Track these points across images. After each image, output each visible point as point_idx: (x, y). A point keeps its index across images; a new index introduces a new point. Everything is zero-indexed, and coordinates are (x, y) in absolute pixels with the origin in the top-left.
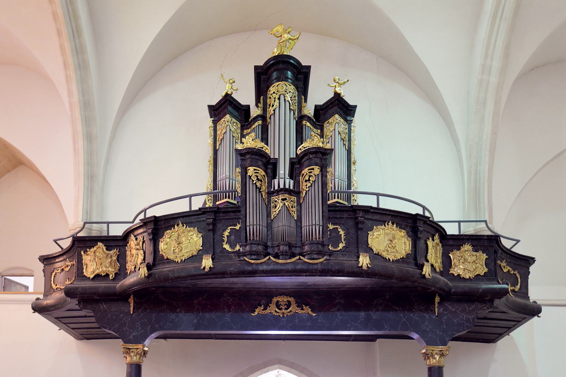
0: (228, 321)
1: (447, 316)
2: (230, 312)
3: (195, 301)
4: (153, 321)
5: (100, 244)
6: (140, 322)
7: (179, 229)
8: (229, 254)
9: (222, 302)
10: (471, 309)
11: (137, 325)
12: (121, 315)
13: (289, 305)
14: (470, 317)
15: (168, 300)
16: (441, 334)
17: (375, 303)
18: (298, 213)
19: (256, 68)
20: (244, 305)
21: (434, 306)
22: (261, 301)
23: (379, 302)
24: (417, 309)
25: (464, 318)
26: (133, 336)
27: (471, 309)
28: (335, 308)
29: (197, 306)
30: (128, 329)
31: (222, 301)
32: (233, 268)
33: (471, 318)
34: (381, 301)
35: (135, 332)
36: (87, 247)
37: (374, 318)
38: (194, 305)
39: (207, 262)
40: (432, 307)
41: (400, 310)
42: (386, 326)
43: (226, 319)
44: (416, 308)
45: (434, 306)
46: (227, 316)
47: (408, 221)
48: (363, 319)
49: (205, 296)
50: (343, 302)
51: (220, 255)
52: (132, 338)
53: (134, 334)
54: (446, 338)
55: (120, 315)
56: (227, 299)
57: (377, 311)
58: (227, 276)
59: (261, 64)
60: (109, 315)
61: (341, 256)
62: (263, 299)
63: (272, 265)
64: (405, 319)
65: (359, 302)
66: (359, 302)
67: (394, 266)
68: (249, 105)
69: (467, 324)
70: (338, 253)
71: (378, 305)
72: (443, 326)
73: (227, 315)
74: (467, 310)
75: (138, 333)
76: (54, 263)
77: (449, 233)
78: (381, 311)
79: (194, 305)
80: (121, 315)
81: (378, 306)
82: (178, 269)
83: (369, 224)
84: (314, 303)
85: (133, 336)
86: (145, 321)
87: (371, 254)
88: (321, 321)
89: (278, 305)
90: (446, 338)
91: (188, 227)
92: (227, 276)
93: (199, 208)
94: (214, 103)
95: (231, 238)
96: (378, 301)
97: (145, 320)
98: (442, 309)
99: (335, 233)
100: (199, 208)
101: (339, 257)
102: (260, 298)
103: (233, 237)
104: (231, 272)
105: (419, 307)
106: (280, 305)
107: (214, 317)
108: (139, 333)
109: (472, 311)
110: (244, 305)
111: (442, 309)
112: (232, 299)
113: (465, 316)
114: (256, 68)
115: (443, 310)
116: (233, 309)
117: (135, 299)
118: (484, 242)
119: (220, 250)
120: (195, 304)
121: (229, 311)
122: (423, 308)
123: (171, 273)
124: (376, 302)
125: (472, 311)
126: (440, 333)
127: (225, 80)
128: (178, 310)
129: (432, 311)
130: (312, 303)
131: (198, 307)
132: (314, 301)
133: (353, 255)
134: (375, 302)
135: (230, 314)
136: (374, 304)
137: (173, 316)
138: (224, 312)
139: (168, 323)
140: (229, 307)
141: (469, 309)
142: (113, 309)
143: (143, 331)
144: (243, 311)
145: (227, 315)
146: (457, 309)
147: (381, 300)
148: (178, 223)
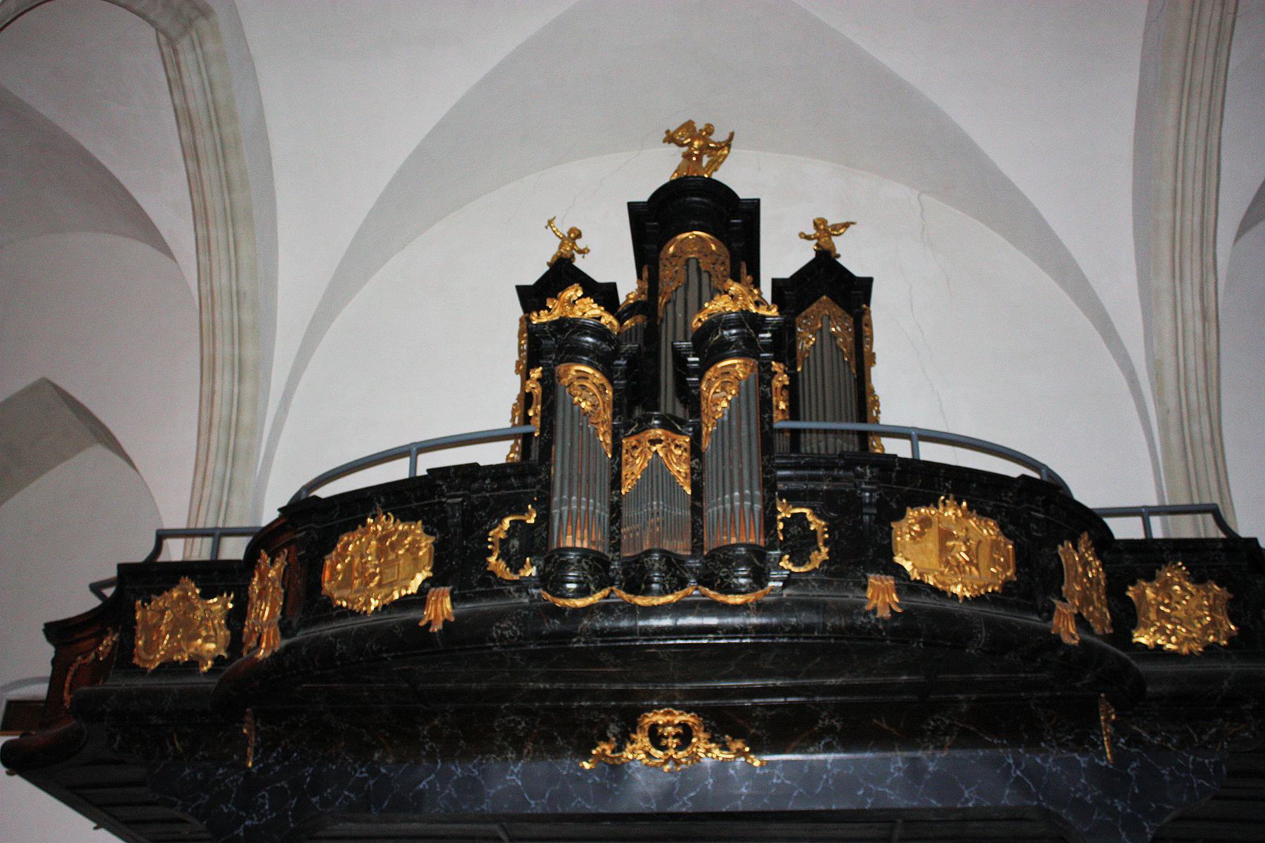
0: (514, 784)
1: (1138, 761)
2: (522, 758)
3: (421, 728)
4: (305, 787)
5: (185, 580)
6: (268, 788)
7: (379, 525)
8: (502, 588)
9: (498, 730)
10: (1205, 738)
11: (260, 797)
12: (221, 771)
13: (685, 736)
14: (1207, 761)
15: (347, 726)
16: (1129, 811)
17: (931, 728)
18: (694, 478)
19: (632, 207)
20: (559, 738)
21: (1099, 733)
22: (607, 727)
23: (943, 723)
24: (1050, 741)
25: (1188, 764)
26: (246, 828)
27: (1205, 738)
28: (817, 744)
29: (428, 742)
30: (234, 809)
31: (498, 726)
32: (509, 622)
33: (1210, 763)
34: (947, 722)
35: (252, 819)
36: (150, 592)
37: (931, 769)
38: (421, 740)
39: (442, 608)
40: (1094, 734)
41: (1004, 746)
42: (966, 792)
43: (508, 778)
44: (1049, 738)
45: (1099, 733)
46: (513, 771)
47: (1001, 497)
48: (901, 774)
49: (447, 711)
50: (838, 725)
51: (478, 589)
52: (242, 834)
53: (248, 823)
54: (1145, 824)
55: (218, 769)
56: (510, 721)
57: (942, 747)
58: (492, 644)
59: (644, 196)
60: (187, 771)
61: (816, 585)
62: (613, 721)
63: (617, 611)
64: (1022, 771)
65: (885, 726)
66: (885, 726)
67: (967, 609)
68: (614, 285)
69: (1199, 781)
70: (807, 580)
71: (940, 733)
72: (1133, 790)
73: (512, 767)
74: (1194, 741)
75: (259, 820)
76: (78, 641)
77: (1118, 535)
78: (952, 747)
79: (421, 740)
80: (221, 771)
81: (941, 735)
82: (359, 629)
83: (892, 503)
84: (757, 728)
85: (246, 828)
86: (283, 787)
87: (901, 582)
88: (779, 781)
89: (656, 737)
90: (1145, 824)
91: (398, 520)
92: (492, 644)
93: (428, 470)
94: (531, 280)
95: (511, 546)
96: (938, 720)
97: (283, 783)
98: (1122, 740)
99: (799, 525)
100: (428, 470)
101: (810, 589)
102: (603, 716)
103: (516, 543)
104: (502, 633)
105: (1058, 735)
106: (662, 736)
107: (477, 773)
108: (264, 820)
109: (1209, 742)
110: (559, 738)
111: (1123, 740)
112: (526, 723)
113: (1191, 758)
114: (632, 207)
115: (1128, 744)
116: (529, 753)
117: (258, 725)
118: (1217, 558)
119: (479, 576)
120: (424, 737)
121: (519, 758)
122: (1070, 738)
123: (340, 642)
124: (932, 723)
125: (1209, 742)
126: (1124, 809)
127: (554, 229)
128: (376, 755)
129: (1095, 745)
130: (753, 731)
131: (431, 747)
132: (757, 724)
133: (851, 584)
134: (929, 724)
135: (520, 765)
136: (928, 730)
137: (362, 773)
138: (503, 759)
139: (346, 793)
140: (518, 746)
141: (1200, 739)
142: (201, 753)
143: (274, 815)
144: (557, 753)
145: (512, 767)
146: (1168, 740)
147: (948, 718)
148: (374, 512)
